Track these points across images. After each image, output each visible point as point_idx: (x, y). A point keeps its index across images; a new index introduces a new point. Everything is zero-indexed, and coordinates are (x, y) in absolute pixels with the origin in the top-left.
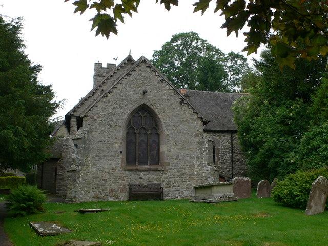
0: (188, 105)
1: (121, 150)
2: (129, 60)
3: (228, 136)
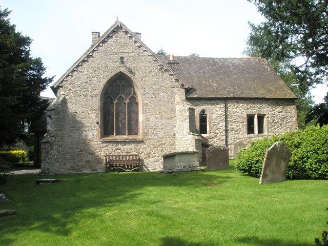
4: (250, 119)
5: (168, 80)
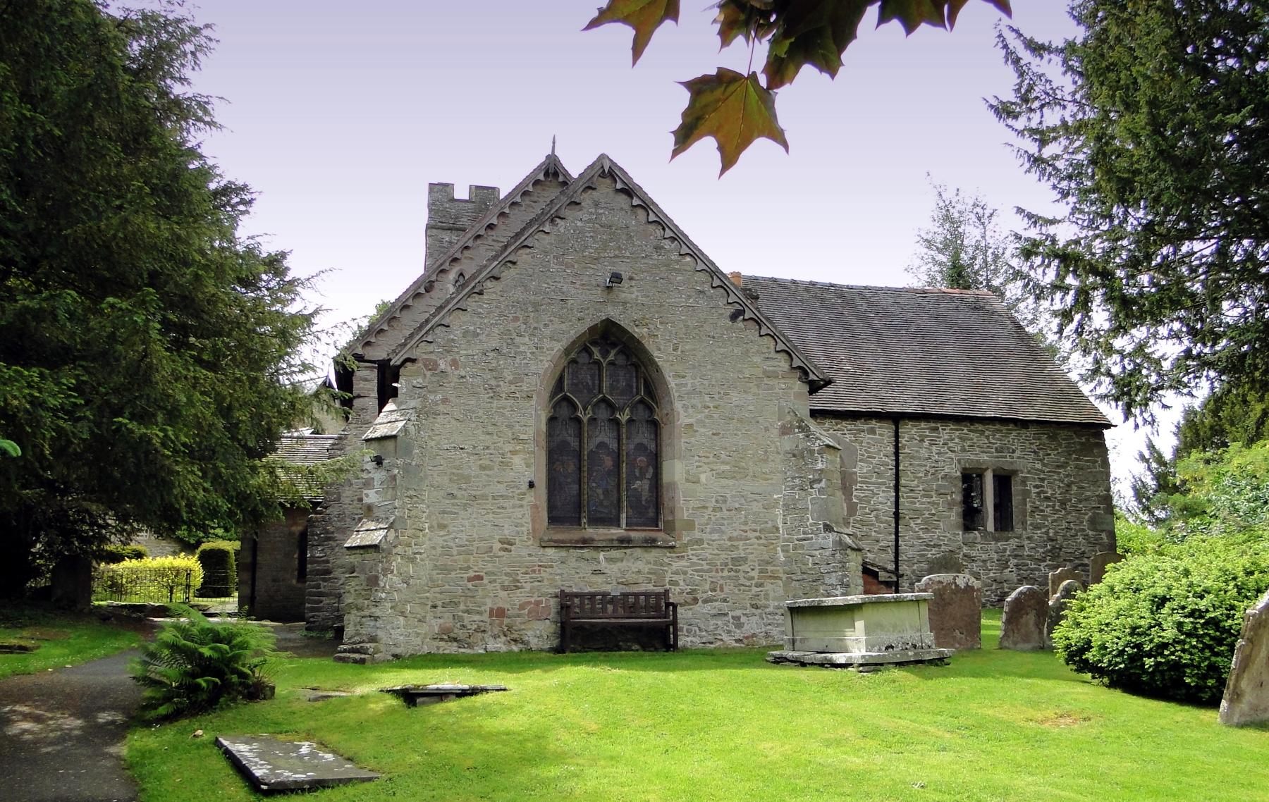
0: (758, 323)
1: (530, 476)
2: (552, 171)
3: (885, 431)
4: (970, 479)
5: (759, 355)
